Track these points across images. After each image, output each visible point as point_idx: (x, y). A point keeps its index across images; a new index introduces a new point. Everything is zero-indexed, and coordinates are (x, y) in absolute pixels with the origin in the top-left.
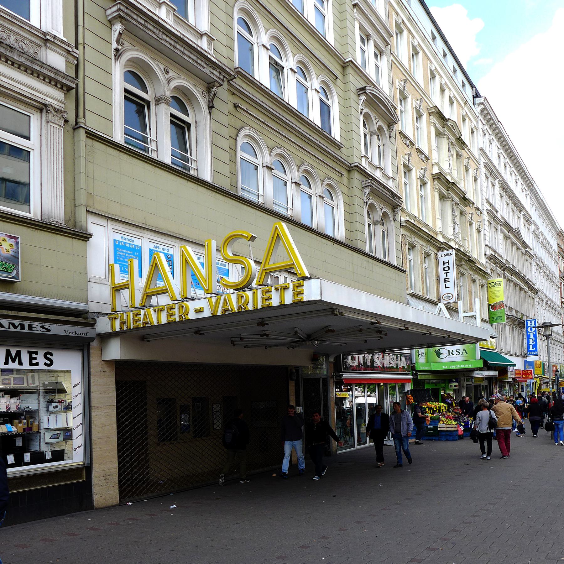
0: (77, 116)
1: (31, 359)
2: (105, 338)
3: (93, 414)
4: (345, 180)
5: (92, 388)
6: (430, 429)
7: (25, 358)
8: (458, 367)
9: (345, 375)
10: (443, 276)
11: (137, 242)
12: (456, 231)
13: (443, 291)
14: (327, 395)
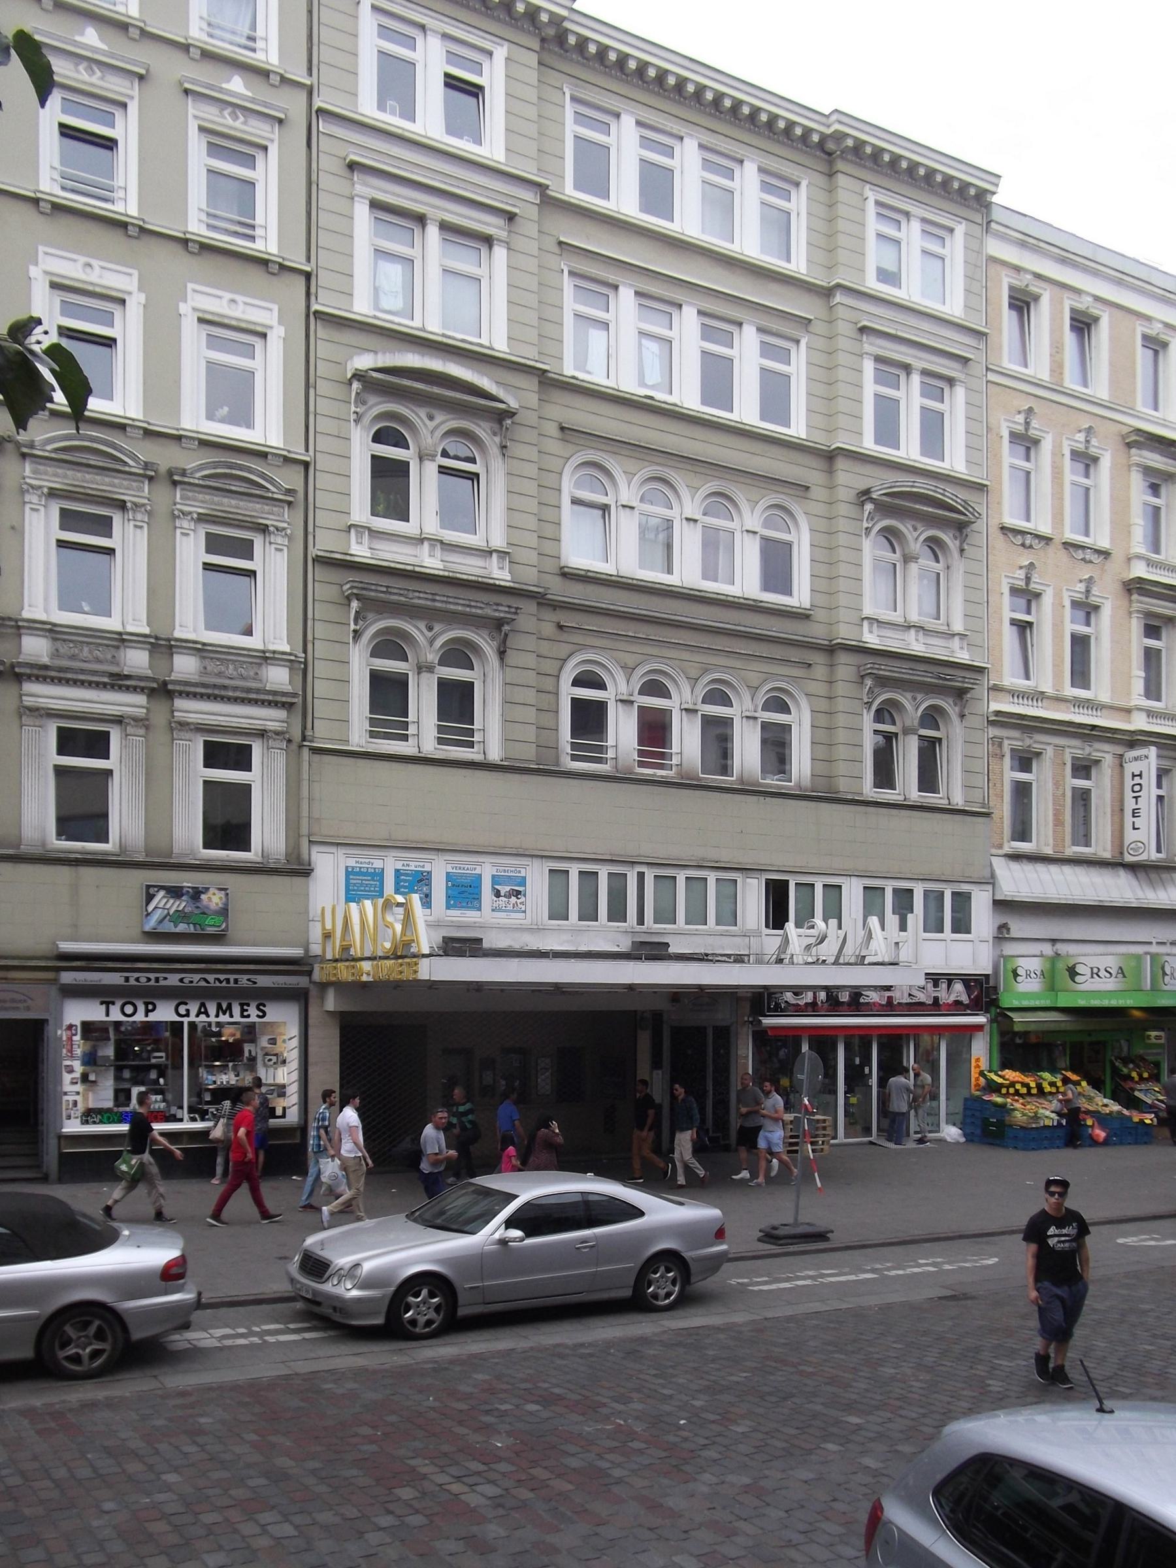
0: (304, 728)
1: (243, 1011)
2: (323, 986)
3: (310, 1071)
4: (820, 672)
5: (310, 1041)
6: (993, 1124)
7: (236, 1010)
8: (1106, 1003)
9: (767, 1021)
10: (1130, 804)
11: (378, 864)
13: (1130, 836)
14: (728, 1053)
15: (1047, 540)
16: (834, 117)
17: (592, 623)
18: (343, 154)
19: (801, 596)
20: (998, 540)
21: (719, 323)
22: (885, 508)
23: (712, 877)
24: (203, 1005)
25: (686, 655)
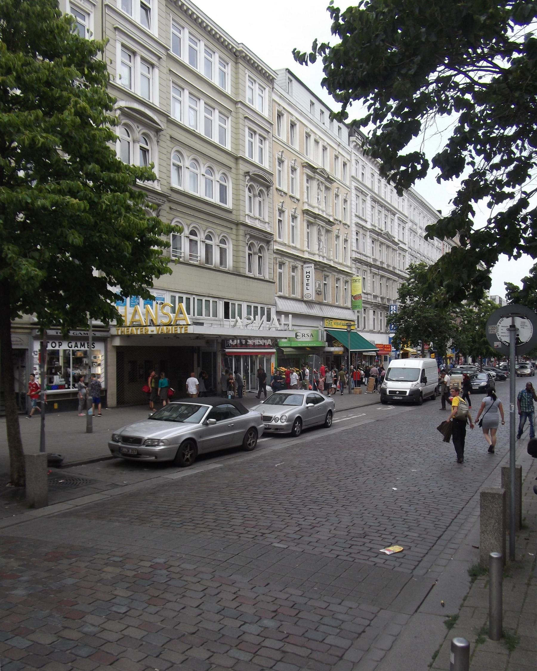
4: (234, 231)
7: (86, 345)
9: (227, 350)
10: (305, 282)
12: (321, 247)
13: (306, 292)
15: (286, 194)
16: (241, 45)
17: (180, 208)
18: (114, 23)
19: (229, 205)
20: (275, 192)
21: (210, 108)
22: (252, 179)
23: (211, 300)
24: (76, 343)
25: (202, 222)
